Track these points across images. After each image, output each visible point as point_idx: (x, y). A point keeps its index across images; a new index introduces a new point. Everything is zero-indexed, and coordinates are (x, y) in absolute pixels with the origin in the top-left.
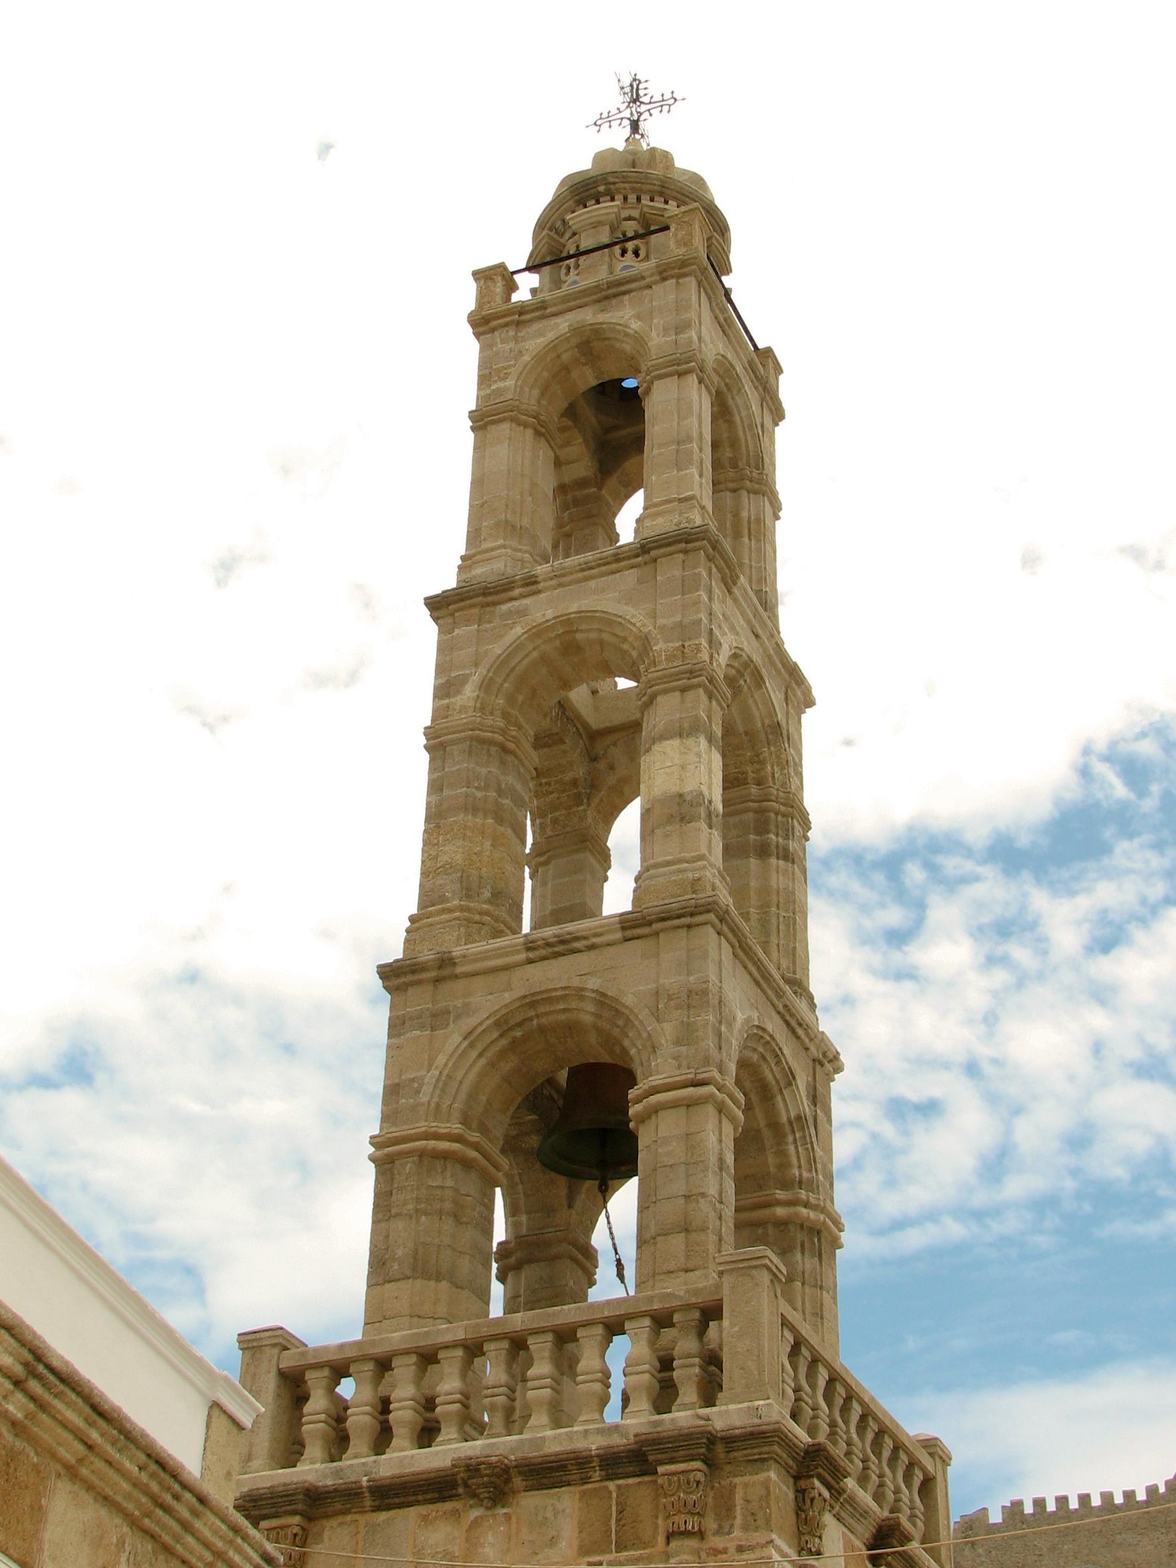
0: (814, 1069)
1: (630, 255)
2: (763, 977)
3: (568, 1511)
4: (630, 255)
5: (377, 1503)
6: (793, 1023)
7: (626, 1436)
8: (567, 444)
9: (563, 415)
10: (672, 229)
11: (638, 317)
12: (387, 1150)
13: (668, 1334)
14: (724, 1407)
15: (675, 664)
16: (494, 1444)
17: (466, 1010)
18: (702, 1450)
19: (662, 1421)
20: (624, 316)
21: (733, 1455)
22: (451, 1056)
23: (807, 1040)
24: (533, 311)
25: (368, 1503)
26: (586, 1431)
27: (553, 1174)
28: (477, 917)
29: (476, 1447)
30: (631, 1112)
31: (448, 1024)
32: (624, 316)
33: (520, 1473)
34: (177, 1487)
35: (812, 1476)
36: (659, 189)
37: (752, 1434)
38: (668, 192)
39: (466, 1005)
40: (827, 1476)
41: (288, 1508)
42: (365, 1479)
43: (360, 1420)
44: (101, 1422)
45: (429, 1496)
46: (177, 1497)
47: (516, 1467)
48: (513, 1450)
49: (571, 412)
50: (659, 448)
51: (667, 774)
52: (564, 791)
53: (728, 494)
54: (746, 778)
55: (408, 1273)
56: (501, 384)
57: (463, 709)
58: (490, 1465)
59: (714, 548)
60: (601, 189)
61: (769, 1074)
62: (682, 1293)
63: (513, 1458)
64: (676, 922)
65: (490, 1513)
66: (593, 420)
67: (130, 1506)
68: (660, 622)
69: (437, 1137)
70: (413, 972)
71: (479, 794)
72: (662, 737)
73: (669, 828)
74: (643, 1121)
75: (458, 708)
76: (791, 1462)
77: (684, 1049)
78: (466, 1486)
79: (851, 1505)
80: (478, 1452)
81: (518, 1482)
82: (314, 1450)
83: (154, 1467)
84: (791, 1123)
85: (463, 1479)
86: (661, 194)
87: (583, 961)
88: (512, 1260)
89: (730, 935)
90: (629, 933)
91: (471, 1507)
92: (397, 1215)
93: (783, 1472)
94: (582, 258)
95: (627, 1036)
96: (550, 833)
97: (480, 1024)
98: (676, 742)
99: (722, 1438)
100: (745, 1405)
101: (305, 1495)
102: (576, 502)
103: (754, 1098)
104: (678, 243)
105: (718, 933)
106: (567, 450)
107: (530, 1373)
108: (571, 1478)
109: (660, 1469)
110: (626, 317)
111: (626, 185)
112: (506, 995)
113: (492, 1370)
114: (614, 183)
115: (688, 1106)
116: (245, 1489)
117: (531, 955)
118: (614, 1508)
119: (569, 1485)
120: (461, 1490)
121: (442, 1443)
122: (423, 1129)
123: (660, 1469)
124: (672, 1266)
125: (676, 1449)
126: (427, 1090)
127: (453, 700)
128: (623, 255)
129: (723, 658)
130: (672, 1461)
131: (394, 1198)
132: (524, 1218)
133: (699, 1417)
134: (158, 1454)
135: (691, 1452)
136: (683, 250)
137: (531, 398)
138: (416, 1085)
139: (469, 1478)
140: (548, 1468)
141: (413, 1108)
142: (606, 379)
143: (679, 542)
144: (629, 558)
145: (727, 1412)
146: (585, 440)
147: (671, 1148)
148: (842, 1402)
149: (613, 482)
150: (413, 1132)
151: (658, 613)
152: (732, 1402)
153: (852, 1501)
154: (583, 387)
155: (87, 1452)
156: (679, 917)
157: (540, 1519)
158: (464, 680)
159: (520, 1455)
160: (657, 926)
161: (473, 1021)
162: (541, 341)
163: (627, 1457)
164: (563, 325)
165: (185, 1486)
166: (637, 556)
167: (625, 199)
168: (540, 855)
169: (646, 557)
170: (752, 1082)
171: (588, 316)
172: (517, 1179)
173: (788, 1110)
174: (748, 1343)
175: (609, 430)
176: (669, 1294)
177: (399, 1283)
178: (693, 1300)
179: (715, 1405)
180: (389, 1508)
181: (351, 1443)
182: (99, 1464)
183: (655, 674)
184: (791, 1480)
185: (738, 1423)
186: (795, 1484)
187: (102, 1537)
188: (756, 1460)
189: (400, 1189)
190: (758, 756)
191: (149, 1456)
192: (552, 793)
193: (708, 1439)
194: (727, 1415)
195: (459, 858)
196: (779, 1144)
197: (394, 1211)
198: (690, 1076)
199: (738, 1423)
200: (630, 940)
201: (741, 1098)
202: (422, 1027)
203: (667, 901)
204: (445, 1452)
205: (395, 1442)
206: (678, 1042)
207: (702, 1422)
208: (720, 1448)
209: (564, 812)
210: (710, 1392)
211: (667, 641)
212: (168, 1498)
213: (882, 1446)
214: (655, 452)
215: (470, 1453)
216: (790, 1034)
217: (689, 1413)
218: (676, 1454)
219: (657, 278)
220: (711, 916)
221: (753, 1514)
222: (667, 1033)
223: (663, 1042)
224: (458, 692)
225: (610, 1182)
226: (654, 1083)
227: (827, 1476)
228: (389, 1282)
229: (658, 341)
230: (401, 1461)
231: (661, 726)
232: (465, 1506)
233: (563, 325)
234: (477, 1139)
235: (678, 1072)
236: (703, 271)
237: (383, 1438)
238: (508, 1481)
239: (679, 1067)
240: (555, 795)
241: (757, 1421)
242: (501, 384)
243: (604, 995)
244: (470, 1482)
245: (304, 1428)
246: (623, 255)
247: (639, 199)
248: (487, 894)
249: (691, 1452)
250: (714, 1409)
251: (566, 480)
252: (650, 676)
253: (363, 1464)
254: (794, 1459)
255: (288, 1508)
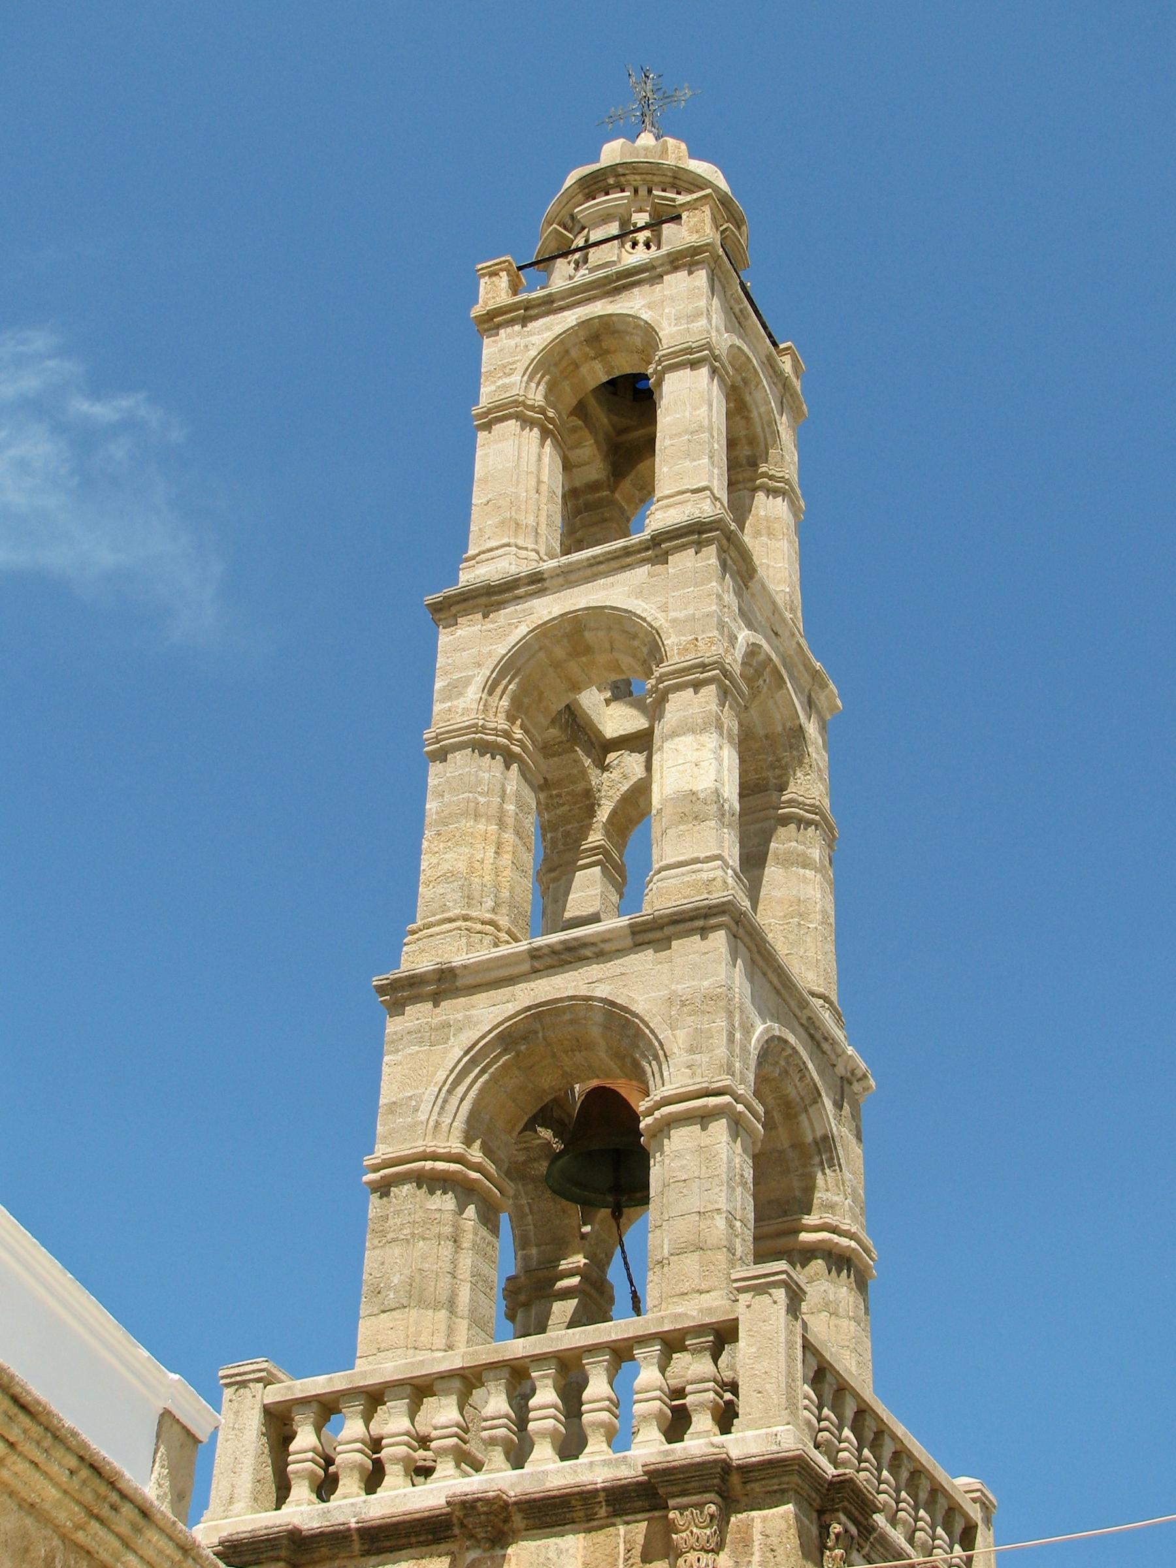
0: (842, 1087)
1: (641, 247)
2: (784, 985)
3: (571, 1551)
4: (641, 247)
5: (366, 1547)
6: (818, 1036)
7: (634, 1467)
8: (578, 445)
9: (571, 414)
10: (684, 217)
11: (649, 306)
12: (382, 1172)
13: (680, 1360)
14: (740, 1435)
15: (687, 658)
16: (493, 1480)
17: (469, 1022)
18: (716, 1481)
19: (673, 1451)
20: (634, 304)
21: (748, 1487)
22: (452, 1071)
23: (833, 1057)
24: (539, 305)
25: (357, 1546)
26: (591, 1463)
27: (564, 1202)
28: (479, 927)
29: (472, 1484)
30: (642, 1125)
31: (448, 1039)
32: (634, 304)
33: (520, 1510)
34: (114, 1497)
35: (837, 1510)
36: (671, 180)
37: (770, 1462)
38: (681, 183)
39: (468, 1018)
40: (853, 1510)
41: (271, 1554)
42: (354, 1520)
43: (350, 1456)
44: (23, 1418)
45: (422, 1539)
46: (114, 1508)
47: (515, 1503)
48: (513, 1485)
49: (580, 410)
50: (671, 438)
51: (678, 771)
52: (575, 804)
53: (746, 492)
54: (767, 784)
55: (405, 1302)
56: (506, 380)
57: (466, 711)
58: (487, 1501)
59: (728, 539)
60: (611, 181)
61: (792, 1090)
62: (695, 1313)
63: (512, 1493)
64: (689, 925)
65: (487, 1554)
66: (605, 420)
67: (61, 1517)
68: (672, 615)
69: (435, 1157)
70: (411, 985)
71: (482, 800)
72: (674, 734)
73: (681, 827)
74: (655, 1136)
75: (460, 711)
76: (814, 1495)
77: (697, 1057)
78: (463, 1525)
79: (882, 1545)
80: (475, 1488)
81: (518, 1521)
82: (301, 1491)
83: (85, 1473)
84: (816, 1143)
85: (459, 1519)
86: (673, 186)
87: (594, 970)
88: (522, 1298)
89: (747, 939)
90: (640, 938)
91: (468, 1549)
92: (394, 1240)
93: (805, 1505)
94: (592, 250)
95: (638, 1047)
96: (561, 847)
97: (483, 1037)
98: (688, 739)
99: (739, 1467)
100: (763, 1431)
101: (289, 1539)
102: (588, 507)
103: (777, 1116)
104: (691, 231)
105: (735, 936)
106: (578, 452)
107: (532, 1402)
108: (575, 1515)
109: (671, 1503)
110: (637, 307)
111: (638, 177)
112: (510, 1005)
113: (495, 1402)
114: (624, 175)
115: (703, 1117)
116: (225, 1534)
117: (537, 964)
118: (622, 1547)
119: (574, 1522)
120: (456, 1531)
121: (436, 1480)
122: (421, 1149)
123: (671, 1503)
124: (686, 1287)
125: (687, 1480)
126: (425, 1107)
127: (455, 703)
128: (633, 248)
129: (739, 652)
130: (684, 1493)
131: (391, 1222)
132: (534, 1251)
133: (713, 1445)
134: (91, 1455)
135: (704, 1483)
136: (695, 237)
137: (537, 395)
138: (414, 1103)
139: (466, 1516)
140: (550, 1504)
141: (412, 1127)
142: (616, 374)
143: (691, 533)
144: (639, 552)
145: (743, 1439)
146: (596, 441)
147: (685, 1162)
148: (872, 1436)
149: (627, 484)
150: (410, 1152)
151: (670, 605)
152: (748, 1428)
153: (883, 1540)
154: (592, 384)
155: (8, 1450)
156: (692, 919)
157: (541, 1560)
158: (467, 681)
159: (519, 1490)
160: (669, 930)
161: (474, 1035)
162: (548, 336)
163: (635, 1491)
164: (570, 318)
165: (124, 1496)
166: (647, 549)
167: (636, 191)
168: (551, 870)
169: (658, 551)
170: (774, 1098)
171: (599, 308)
172: (527, 1209)
173: (813, 1131)
174: (765, 1364)
175: (620, 432)
176: (680, 1315)
177: (394, 1313)
178: (707, 1320)
179: (730, 1433)
180: (379, 1552)
181: (341, 1483)
182: (21, 1466)
183: (667, 669)
184: (815, 1515)
185: (755, 1451)
186: (819, 1518)
187: (27, 1550)
188: (775, 1492)
189: (398, 1213)
190: (779, 760)
191: (81, 1458)
192: (563, 804)
193: (723, 1469)
194: (746, 1443)
195: (462, 866)
196: (804, 1166)
197: (390, 1236)
198: (704, 1085)
199: (754, 1450)
200: (640, 945)
201: (760, 1109)
202: (420, 1042)
203: (679, 903)
204: (440, 1489)
205: (387, 1481)
206: (692, 1050)
207: (717, 1450)
208: (735, 1479)
209: (576, 825)
210: (726, 1418)
211: (680, 633)
212: (105, 1512)
213: (918, 1487)
214: (667, 442)
215: (467, 1489)
216: (815, 1048)
217: (702, 1441)
218: (689, 1486)
219: (668, 267)
220: (724, 919)
221: (772, 1550)
222: (680, 1042)
223: (676, 1050)
224: (461, 694)
225: (625, 1210)
226: (666, 1094)
227: (853, 1510)
228: (384, 1312)
229: (670, 335)
230: (393, 1500)
231: (674, 722)
232: (461, 1547)
233: (570, 318)
234: (480, 1160)
235: (691, 1081)
236: (716, 259)
237: (373, 1479)
238: (506, 1520)
239: (694, 1074)
240: (566, 808)
241: (775, 1448)
242: (506, 380)
243: (613, 1004)
244: (465, 1521)
245: (290, 1468)
246: (633, 248)
247: (650, 191)
248: (490, 904)
249: (704, 1483)
250: (729, 1436)
251: (578, 484)
252: (662, 670)
253: (352, 1504)
254: (817, 1491)
255: (271, 1554)
